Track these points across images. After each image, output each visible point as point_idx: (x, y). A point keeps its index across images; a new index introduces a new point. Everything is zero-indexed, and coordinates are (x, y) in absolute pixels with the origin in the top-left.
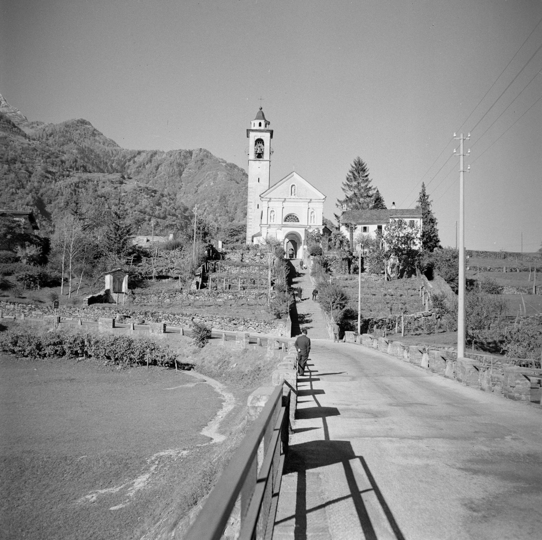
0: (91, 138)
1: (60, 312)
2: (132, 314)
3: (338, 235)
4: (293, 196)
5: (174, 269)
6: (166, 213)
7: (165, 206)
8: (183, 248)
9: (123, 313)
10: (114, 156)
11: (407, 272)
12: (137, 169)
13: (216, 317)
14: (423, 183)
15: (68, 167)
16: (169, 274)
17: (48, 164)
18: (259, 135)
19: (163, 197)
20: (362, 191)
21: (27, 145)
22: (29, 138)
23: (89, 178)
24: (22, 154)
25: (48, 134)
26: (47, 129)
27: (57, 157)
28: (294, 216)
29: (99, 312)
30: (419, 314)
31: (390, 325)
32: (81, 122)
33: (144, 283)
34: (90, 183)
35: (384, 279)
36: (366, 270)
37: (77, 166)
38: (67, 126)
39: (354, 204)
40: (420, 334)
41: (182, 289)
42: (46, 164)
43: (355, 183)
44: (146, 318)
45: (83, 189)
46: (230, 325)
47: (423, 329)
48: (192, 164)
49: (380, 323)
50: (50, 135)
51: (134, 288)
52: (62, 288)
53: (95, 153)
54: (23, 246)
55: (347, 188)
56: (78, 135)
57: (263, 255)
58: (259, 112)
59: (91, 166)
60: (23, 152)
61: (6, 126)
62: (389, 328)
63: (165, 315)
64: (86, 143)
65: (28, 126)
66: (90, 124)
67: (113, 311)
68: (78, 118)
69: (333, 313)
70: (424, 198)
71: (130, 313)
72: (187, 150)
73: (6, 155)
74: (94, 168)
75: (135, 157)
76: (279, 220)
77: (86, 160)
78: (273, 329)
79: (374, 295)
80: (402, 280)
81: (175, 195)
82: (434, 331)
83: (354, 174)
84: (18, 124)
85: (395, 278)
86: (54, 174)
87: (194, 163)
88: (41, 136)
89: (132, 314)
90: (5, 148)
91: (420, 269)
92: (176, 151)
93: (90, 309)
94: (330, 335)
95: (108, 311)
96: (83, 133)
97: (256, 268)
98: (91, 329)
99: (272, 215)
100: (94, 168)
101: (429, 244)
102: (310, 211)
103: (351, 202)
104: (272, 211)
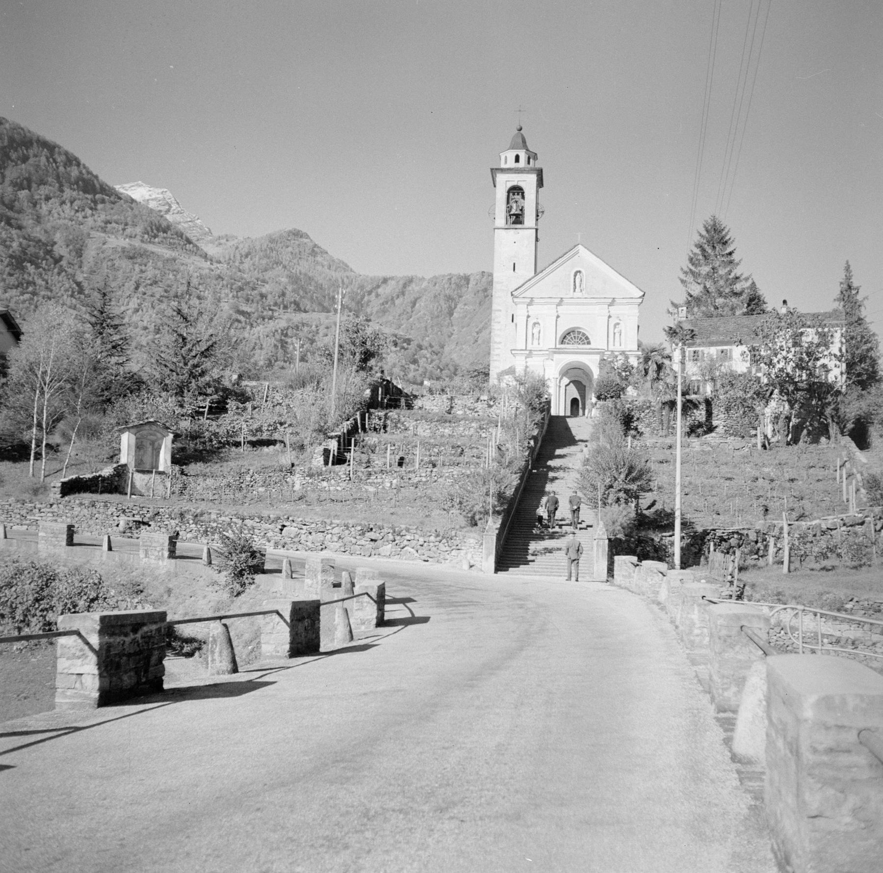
0: (309, 259)
2: (153, 518)
3: (652, 352)
4: (578, 294)
5: (286, 425)
7: (425, 365)
9: (134, 515)
12: (382, 307)
13: (331, 523)
14: (847, 262)
16: (276, 436)
17: (240, 299)
18: (514, 179)
20: (722, 283)
21: (207, 271)
22: (211, 260)
23: (304, 321)
24: (199, 284)
25: (244, 254)
26: (241, 246)
27: (253, 289)
28: (579, 333)
29: (82, 513)
30: (831, 520)
31: (759, 544)
32: (294, 234)
33: (222, 455)
34: (306, 329)
35: (755, 445)
36: (717, 430)
37: (285, 303)
38: (272, 241)
39: (704, 309)
40: (833, 568)
41: (293, 465)
42: (236, 299)
43: (705, 269)
44: (183, 527)
46: (363, 542)
47: (839, 555)
48: (468, 296)
49: (733, 541)
50: (247, 256)
55: (690, 278)
56: (289, 254)
57: (493, 399)
60: (201, 282)
61: (176, 241)
62: (757, 553)
63: (223, 518)
64: (303, 267)
65: (212, 242)
66: (307, 237)
67: (112, 509)
68: (290, 228)
70: (848, 293)
71: (148, 515)
72: (462, 274)
73: (175, 286)
74: (314, 305)
75: (378, 287)
76: (550, 340)
77: (301, 293)
78: (454, 553)
79: (730, 479)
80: (796, 447)
82: (870, 559)
84: (198, 240)
85: (780, 445)
86: (250, 316)
88: (232, 258)
89: (153, 518)
90: (173, 275)
91: (837, 423)
92: (444, 276)
95: (101, 510)
96: (297, 251)
97: (473, 425)
98: (24, 548)
99: (536, 331)
100: (314, 305)
101: (858, 368)
102: (613, 321)
103: (698, 306)
104: (535, 324)
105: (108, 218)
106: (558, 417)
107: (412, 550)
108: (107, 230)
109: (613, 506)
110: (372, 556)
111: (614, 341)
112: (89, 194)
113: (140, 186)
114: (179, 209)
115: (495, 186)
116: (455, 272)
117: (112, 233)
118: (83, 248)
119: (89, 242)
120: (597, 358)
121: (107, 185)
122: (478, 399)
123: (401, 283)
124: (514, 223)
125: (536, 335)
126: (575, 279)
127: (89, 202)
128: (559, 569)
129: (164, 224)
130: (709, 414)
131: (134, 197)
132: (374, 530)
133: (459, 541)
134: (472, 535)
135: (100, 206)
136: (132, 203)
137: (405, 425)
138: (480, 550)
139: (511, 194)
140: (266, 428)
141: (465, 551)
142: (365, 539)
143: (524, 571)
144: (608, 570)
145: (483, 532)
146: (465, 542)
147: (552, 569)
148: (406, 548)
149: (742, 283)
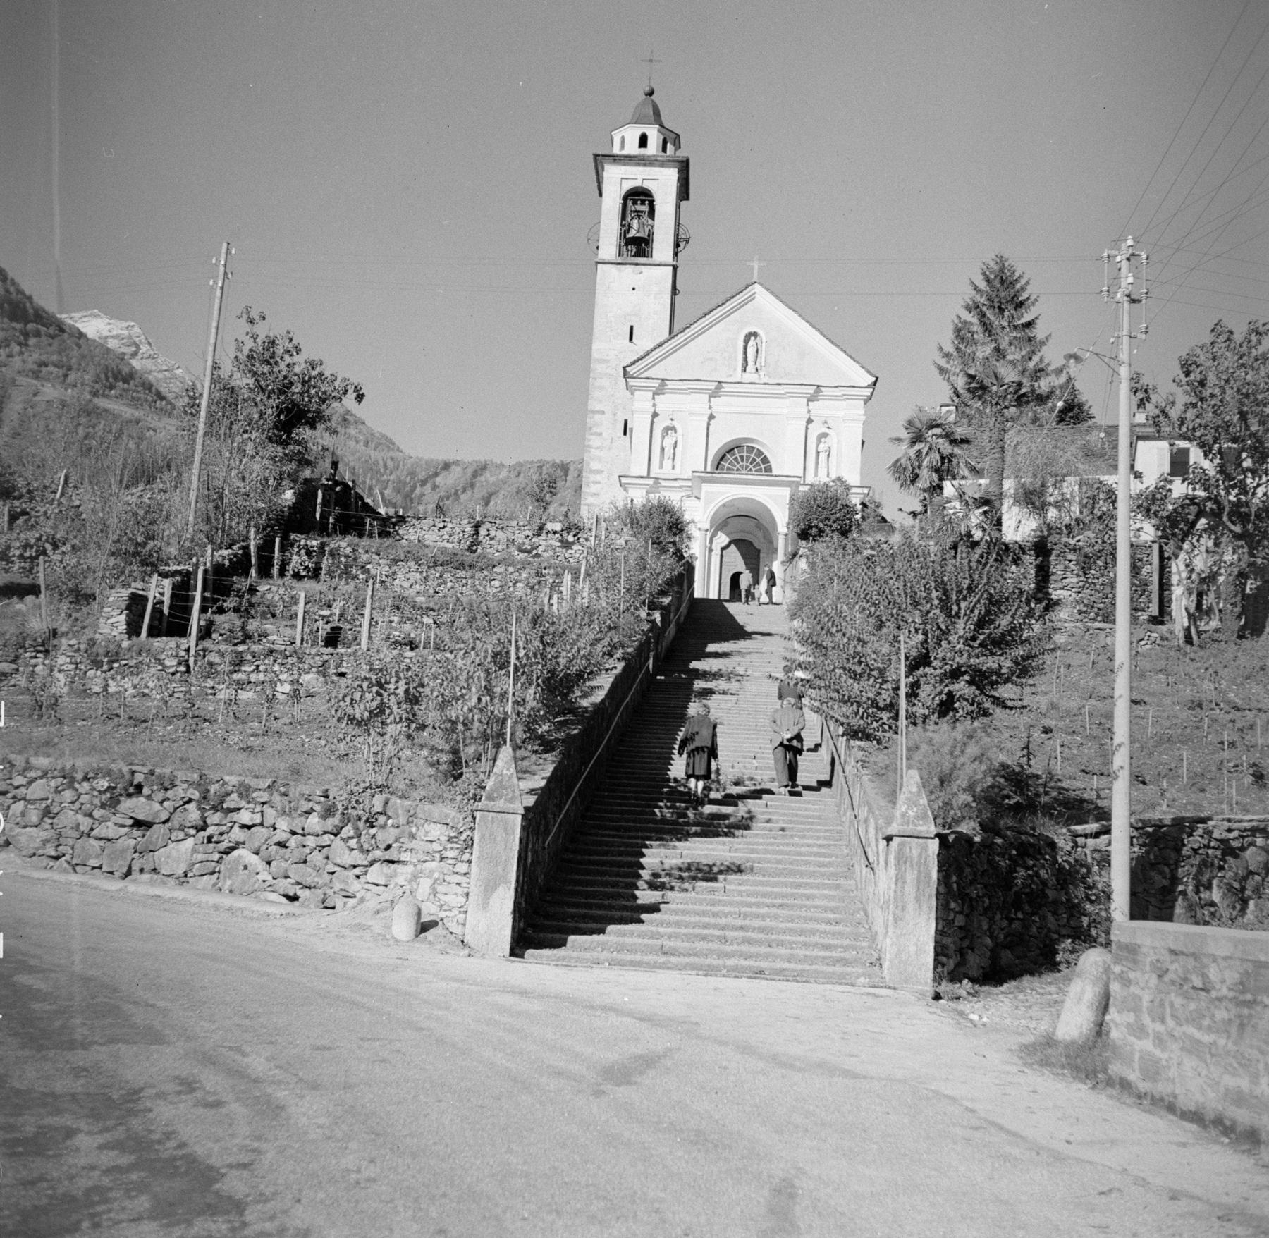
3: (931, 427)
4: (750, 376)
10: (388, 472)
18: (637, 176)
28: (751, 449)
46: (109, 830)
58: (643, 103)
69: (912, 749)
72: (558, 461)
75: (436, 474)
78: (375, 874)
84: (176, 397)
92: (532, 462)
94: (888, 946)
99: (668, 442)
104: (667, 429)
105: (44, 358)
106: (707, 601)
107: (254, 859)
108: (41, 375)
109: (931, 726)
110: (135, 875)
111: (817, 463)
112: (17, 321)
113: (96, 316)
114: (152, 352)
115: (601, 195)
116: (548, 458)
117: (48, 380)
118: (5, 400)
119: (14, 392)
120: (786, 492)
121: (44, 311)
122: (541, 528)
123: (470, 471)
124: (637, 255)
125: (669, 451)
126: (745, 348)
127: (18, 334)
128: (749, 941)
129: (126, 370)
130: (1043, 574)
131: (84, 330)
132: (146, 791)
133: (393, 832)
134: (437, 810)
135: (32, 341)
136: (79, 338)
137: (368, 571)
138: (462, 868)
139: (630, 203)
140: (18, 553)
141: (409, 869)
142: (119, 819)
143: (621, 948)
144: (937, 954)
145: (476, 798)
146: (413, 836)
147: (724, 940)
148: (235, 853)
149: (1049, 379)
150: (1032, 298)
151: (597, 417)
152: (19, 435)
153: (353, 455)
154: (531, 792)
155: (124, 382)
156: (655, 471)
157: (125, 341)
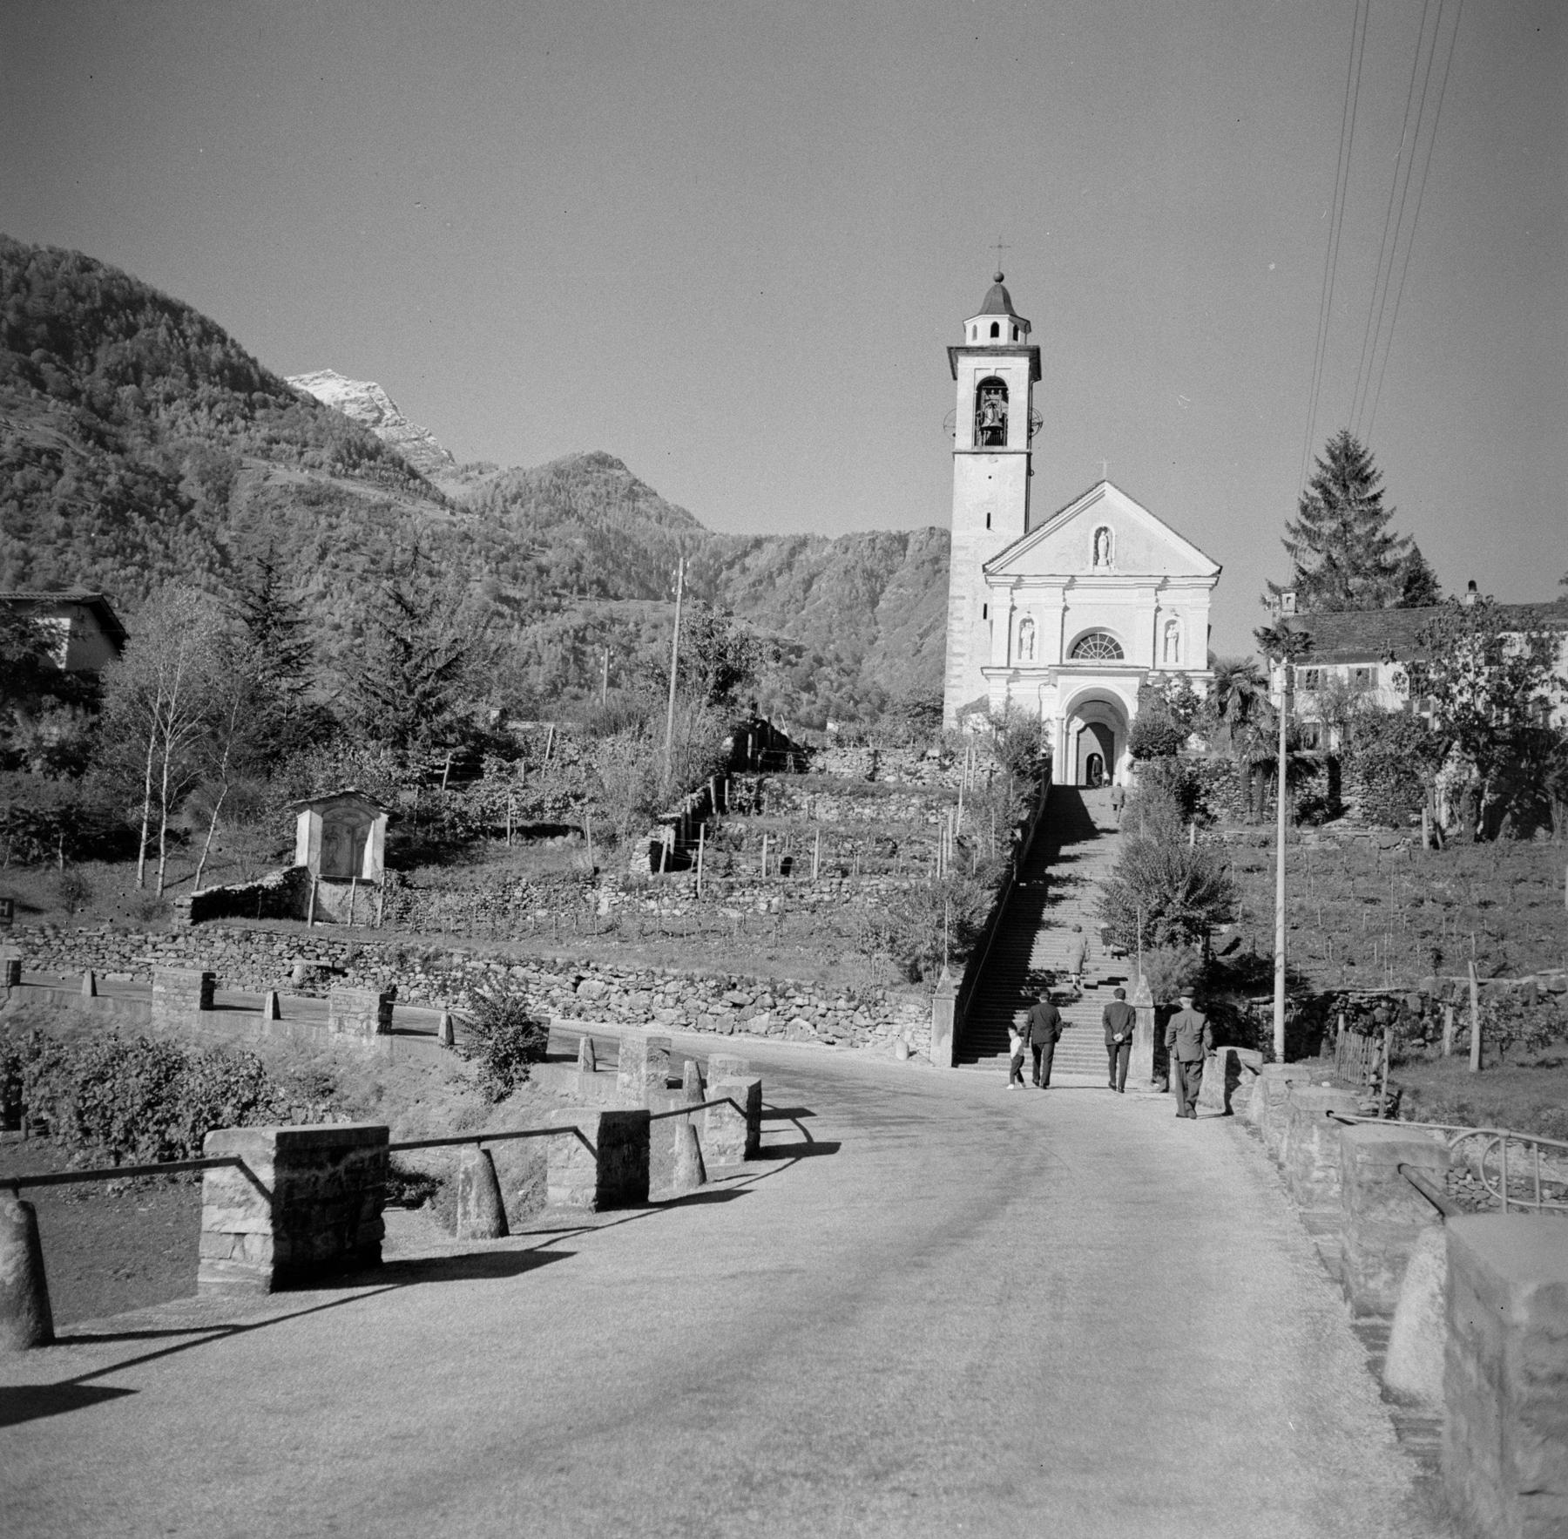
1: (85, 949)
2: (350, 962)
3: (1233, 672)
4: (1102, 568)
6: (828, 710)
7: (827, 693)
8: (647, 730)
9: (318, 957)
10: (687, 553)
11: (1514, 814)
13: (664, 974)
15: (558, 584)
16: (568, 819)
19: (821, 665)
20: (1359, 549)
21: (446, 526)
22: (453, 508)
23: (615, 616)
24: (431, 549)
25: (508, 496)
26: (504, 483)
27: (526, 558)
28: (1103, 637)
31: (1426, 1019)
32: (598, 461)
35: (1418, 841)
41: (597, 871)
42: (495, 576)
43: (1329, 526)
44: (405, 978)
45: (597, 647)
46: (718, 1008)
48: (905, 572)
50: (514, 501)
51: (412, 868)
52: (141, 862)
53: (635, 547)
54: (33, 713)
55: (1303, 542)
57: (949, 754)
58: (994, 289)
59: (623, 583)
60: (435, 545)
62: (1422, 1035)
63: (474, 963)
64: (613, 519)
65: (454, 475)
66: (621, 466)
67: (281, 946)
68: (590, 450)
71: (343, 957)
72: (894, 532)
73: (389, 553)
74: (632, 587)
75: (746, 554)
76: (1050, 651)
77: (610, 565)
78: (880, 1029)
79: (1372, 901)
80: (1492, 846)
81: (859, 661)
83: (1326, 492)
85: (1463, 840)
86: (519, 605)
87: (911, 569)
88: (489, 502)
89: (350, 962)
93: (199, 940)
95: (262, 948)
96: (603, 491)
97: (914, 801)
99: (1026, 634)
100: (632, 587)
102: (1163, 618)
103: (1317, 591)
104: (1024, 622)
105: (274, 433)
106: (1065, 788)
108: (272, 454)
109: (1163, 948)
111: (1166, 648)
112: (240, 390)
113: (330, 377)
114: (398, 418)
117: (280, 460)
119: (241, 476)
120: (1135, 682)
121: (272, 376)
122: (923, 755)
123: (786, 547)
124: (989, 443)
125: (1027, 642)
126: (1096, 542)
127: (241, 406)
129: (371, 444)
130: (1335, 785)
131: (318, 396)
132: (738, 987)
133: (889, 1009)
134: (912, 997)
135: (259, 413)
139: (984, 393)
140: (550, 805)
142: (723, 1002)
146: (900, 1011)
148: (794, 1021)
149: (1395, 551)
150: (1378, 472)
151: (958, 602)
152: (250, 527)
153: (644, 534)
154: (956, 987)
155: (370, 460)
156: (1015, 662)
157: (365, 405)
